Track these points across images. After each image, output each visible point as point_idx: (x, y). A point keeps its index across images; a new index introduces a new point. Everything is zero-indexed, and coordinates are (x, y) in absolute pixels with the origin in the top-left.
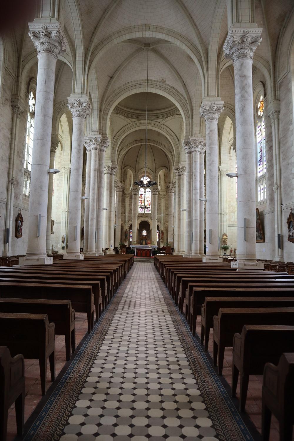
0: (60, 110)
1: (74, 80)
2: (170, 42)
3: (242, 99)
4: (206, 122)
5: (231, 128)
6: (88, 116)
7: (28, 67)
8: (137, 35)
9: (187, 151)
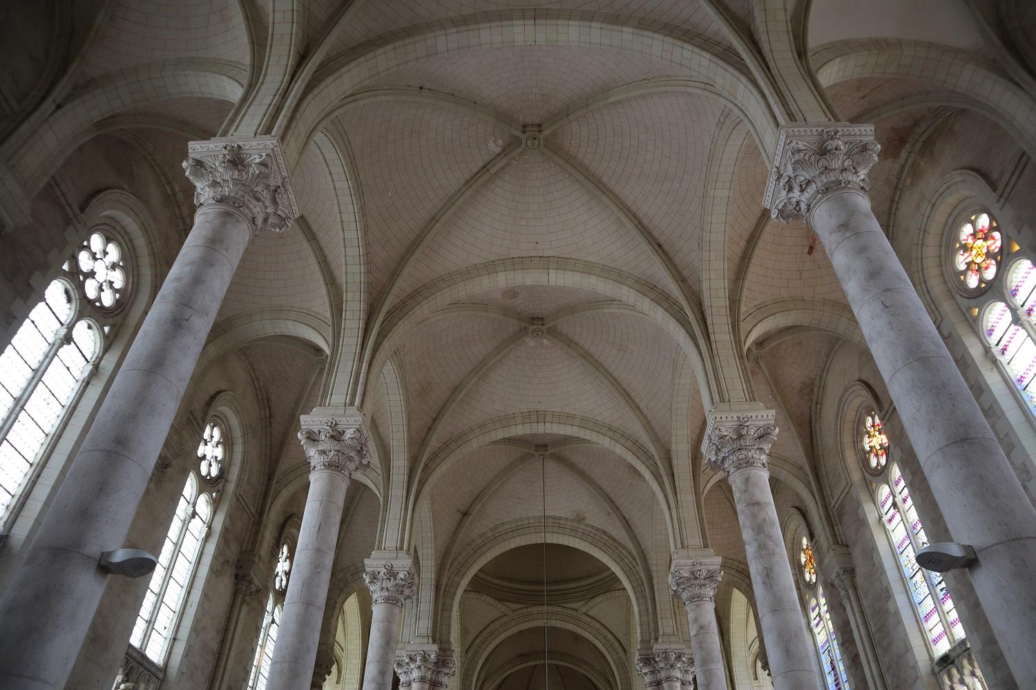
0: (346, 586)
1: (382, 521)
2: (585, 441)
4: (687, 608)
5: (748, 615)
6: (408, 601)
7: (286, 493)
8: (520, 430)
9: (647, 679)
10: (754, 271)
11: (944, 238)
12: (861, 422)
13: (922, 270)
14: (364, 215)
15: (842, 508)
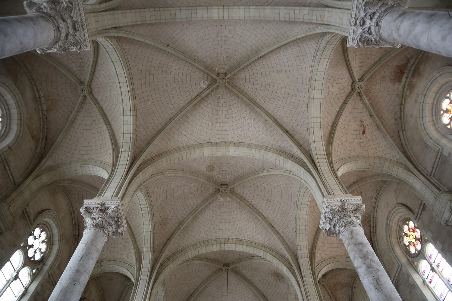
1: (133, 293)
3: (371, 270)
10: (336, 143)
11: (434, 111)
12: (401, 230)
13: (425, 129)
14: (135, 110)
15: (398, 282)
